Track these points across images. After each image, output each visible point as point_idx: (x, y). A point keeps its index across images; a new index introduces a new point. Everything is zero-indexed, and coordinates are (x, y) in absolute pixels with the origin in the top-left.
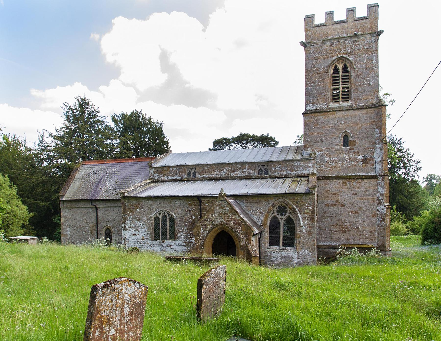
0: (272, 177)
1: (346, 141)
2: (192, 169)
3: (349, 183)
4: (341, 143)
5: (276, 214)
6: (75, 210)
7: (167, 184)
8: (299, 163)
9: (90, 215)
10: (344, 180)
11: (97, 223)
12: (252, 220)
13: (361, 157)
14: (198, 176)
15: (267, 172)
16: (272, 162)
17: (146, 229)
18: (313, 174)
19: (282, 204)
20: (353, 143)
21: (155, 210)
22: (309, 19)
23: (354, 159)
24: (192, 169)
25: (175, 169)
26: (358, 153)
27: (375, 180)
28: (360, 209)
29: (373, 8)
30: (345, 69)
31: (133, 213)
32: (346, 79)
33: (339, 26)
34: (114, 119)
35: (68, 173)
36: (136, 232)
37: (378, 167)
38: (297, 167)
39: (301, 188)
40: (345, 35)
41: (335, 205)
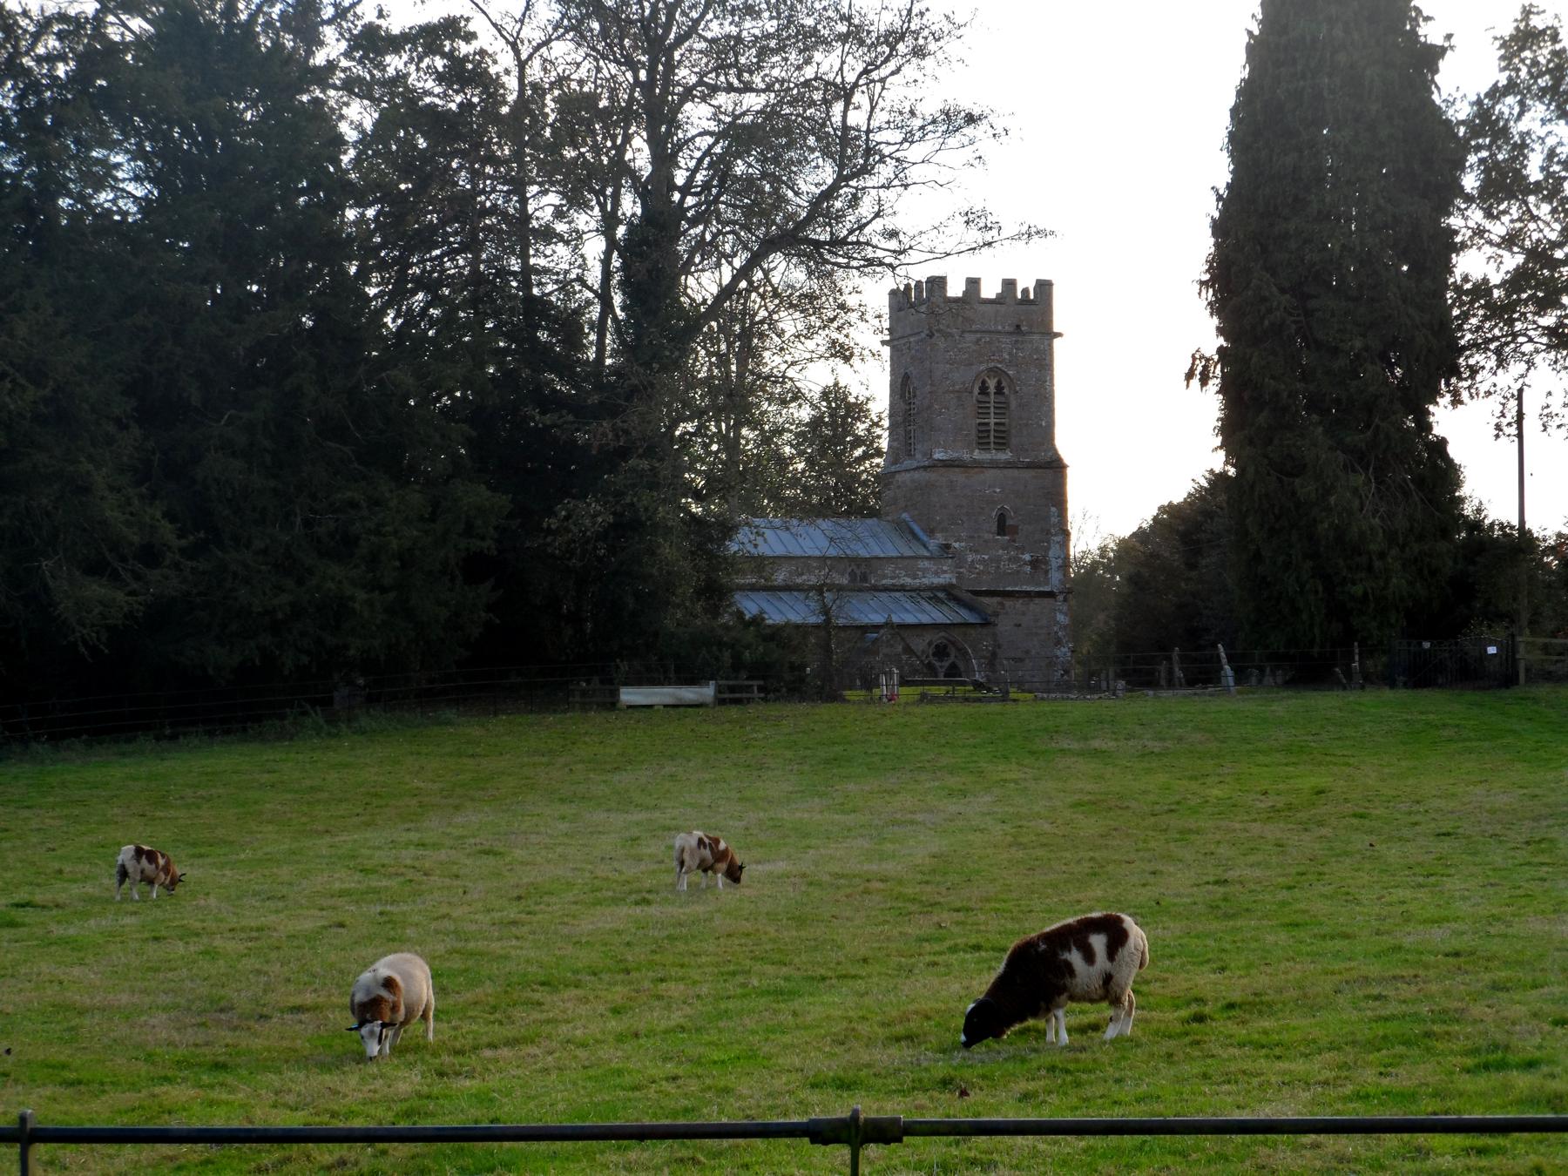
0: (875, 589)
1: (1002, 528)
4: (994, 528)
8: (926, 563)
13: (1027, 557)
15: (864, 578)
23: (1016, 560)
26: (1022, 550)
27: (1051, 601)
28: (1027, 652)
30: (999, 390)
32: (1002, 408)
38: (924, 570)
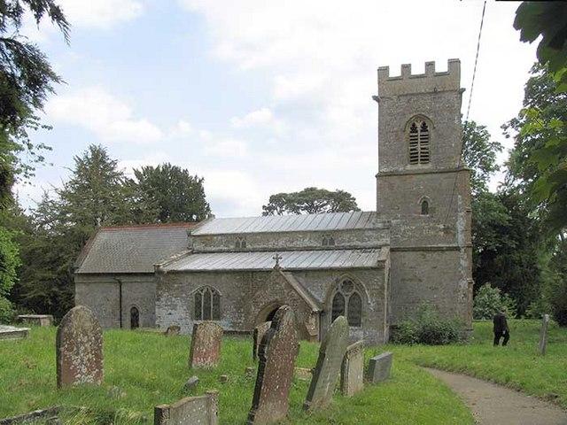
0: (338, 249)
1: (425, 210)
2: (241, 239)
3: (429, 255)
5: (340, 290)
6: (93, 285)
7: (211, 255)
9: (114, 291)
10: (422, 252)
11: (121, 301)
12: (311, 296)
13: (442, 227)
14: (249, 246)
15: (332, 242)
16: (338, 231)
17: (185, 307)
18: (386, 245)
19: (348, 277)
20: (434, 210)
21: (198, 285)
22: (383, 71)
23: (434, 228)
24: (241, 239)
25: (220, 238)
26: (438, 222)
27: (457, 252)
29: (454, 64)
30: (424, 128)
31: (169, 289)
32: (425, 139)
33: (416, 81)
34: (137, 173)
35: (80, 241)
36: (174, 313)
37: (460, 237)
39: (368, 260)
40: (423, 91)
41: (411, 280)
